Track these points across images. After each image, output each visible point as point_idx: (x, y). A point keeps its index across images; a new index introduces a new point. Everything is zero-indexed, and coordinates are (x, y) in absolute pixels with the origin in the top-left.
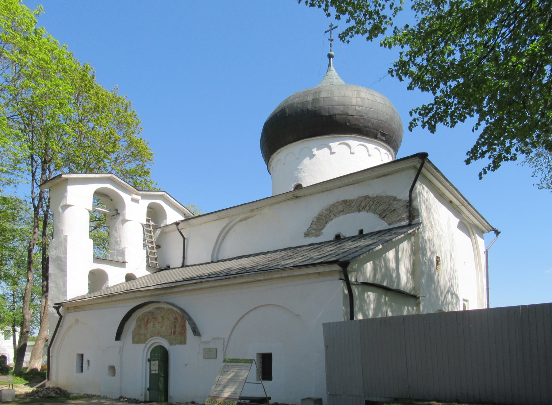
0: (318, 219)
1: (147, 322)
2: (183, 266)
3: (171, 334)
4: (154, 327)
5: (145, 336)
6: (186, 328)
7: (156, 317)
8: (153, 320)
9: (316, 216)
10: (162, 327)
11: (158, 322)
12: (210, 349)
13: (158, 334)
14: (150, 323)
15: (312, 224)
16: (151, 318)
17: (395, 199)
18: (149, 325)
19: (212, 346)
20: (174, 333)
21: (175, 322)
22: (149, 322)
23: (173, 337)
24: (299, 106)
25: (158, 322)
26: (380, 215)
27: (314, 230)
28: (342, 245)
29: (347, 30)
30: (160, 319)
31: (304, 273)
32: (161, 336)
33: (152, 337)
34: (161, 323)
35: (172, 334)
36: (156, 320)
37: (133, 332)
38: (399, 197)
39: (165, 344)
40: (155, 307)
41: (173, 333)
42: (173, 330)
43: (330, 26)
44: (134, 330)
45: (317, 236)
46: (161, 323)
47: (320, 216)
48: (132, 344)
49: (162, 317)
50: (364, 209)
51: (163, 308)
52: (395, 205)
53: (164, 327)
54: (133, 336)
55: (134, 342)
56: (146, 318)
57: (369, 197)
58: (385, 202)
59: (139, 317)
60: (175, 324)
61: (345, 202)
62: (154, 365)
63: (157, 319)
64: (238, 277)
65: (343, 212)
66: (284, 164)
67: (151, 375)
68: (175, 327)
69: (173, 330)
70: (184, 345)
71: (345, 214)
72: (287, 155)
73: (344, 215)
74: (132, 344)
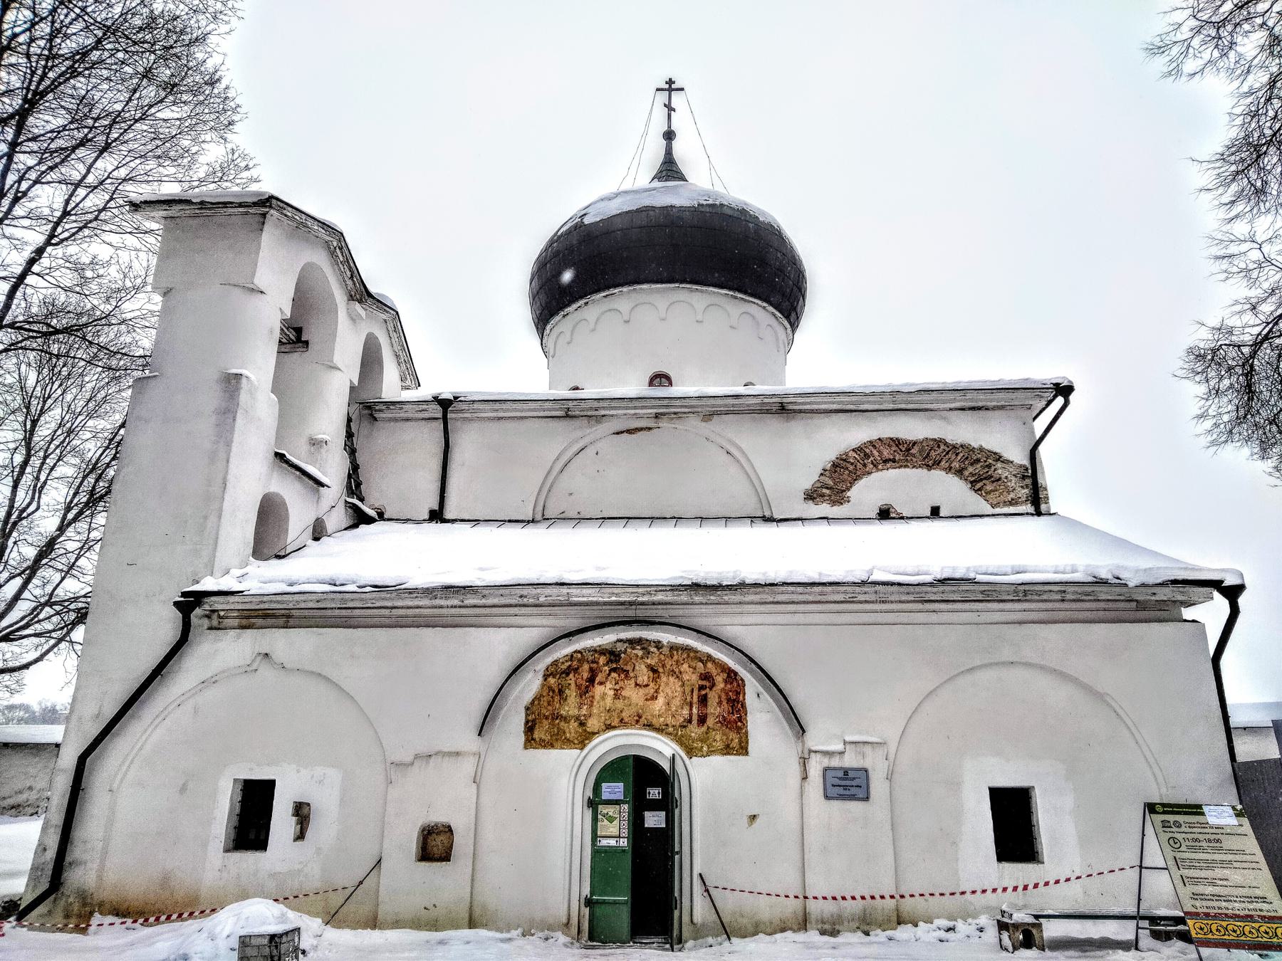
0: (835, 465)
1: (591, 680)
2: (437, 516)
3: (690, 721)
4: (617, 696)
5: (582, 724)
7: (629, 668)
8: (614, 675)
9: (834, 459)
10: (654, 698)
11: (637, 685)
12: (846, 772)
14: (601, 683)
15: (822, 474)
17: (998, 458)
18: (598, 690)
19: (850, 761)
20: (702, 720)
21: (701, 688)
22: (598, 680)
23: (695, 731)
25: (637, 685)
26: (973, 483)
27: (827, 488)
30: (643, 675)
32: (649, 726)
33: (609, 727)
35: (695, 721)
36: (627, 677)
38: (1007, 455)
39: (661, 748)
41: (695, 718)
42: (695, 711)
43: (667, 83)
45: (834, 503)
47: (842, 459)
48: (526, 748)
49: (653, 670)
50: (938, 465)
51: (658, 645)
52: (1001, 471)
53: (661, 700)
55: (531, 740)
56: (586, 667)
57: (946, 444)
58: (978, 461)
59: (555, 663)
60: (703, 692)
61: (897, 442)
62: (611, 819)
65: (889, 462)
66: (627, 322)
67: (597, 852)
68: (703, 701)
69: (695, 711)
70: (740, 759)
71: (899, 467)
72: (636, 306)
73: (897, 470)
74: (526, 748)
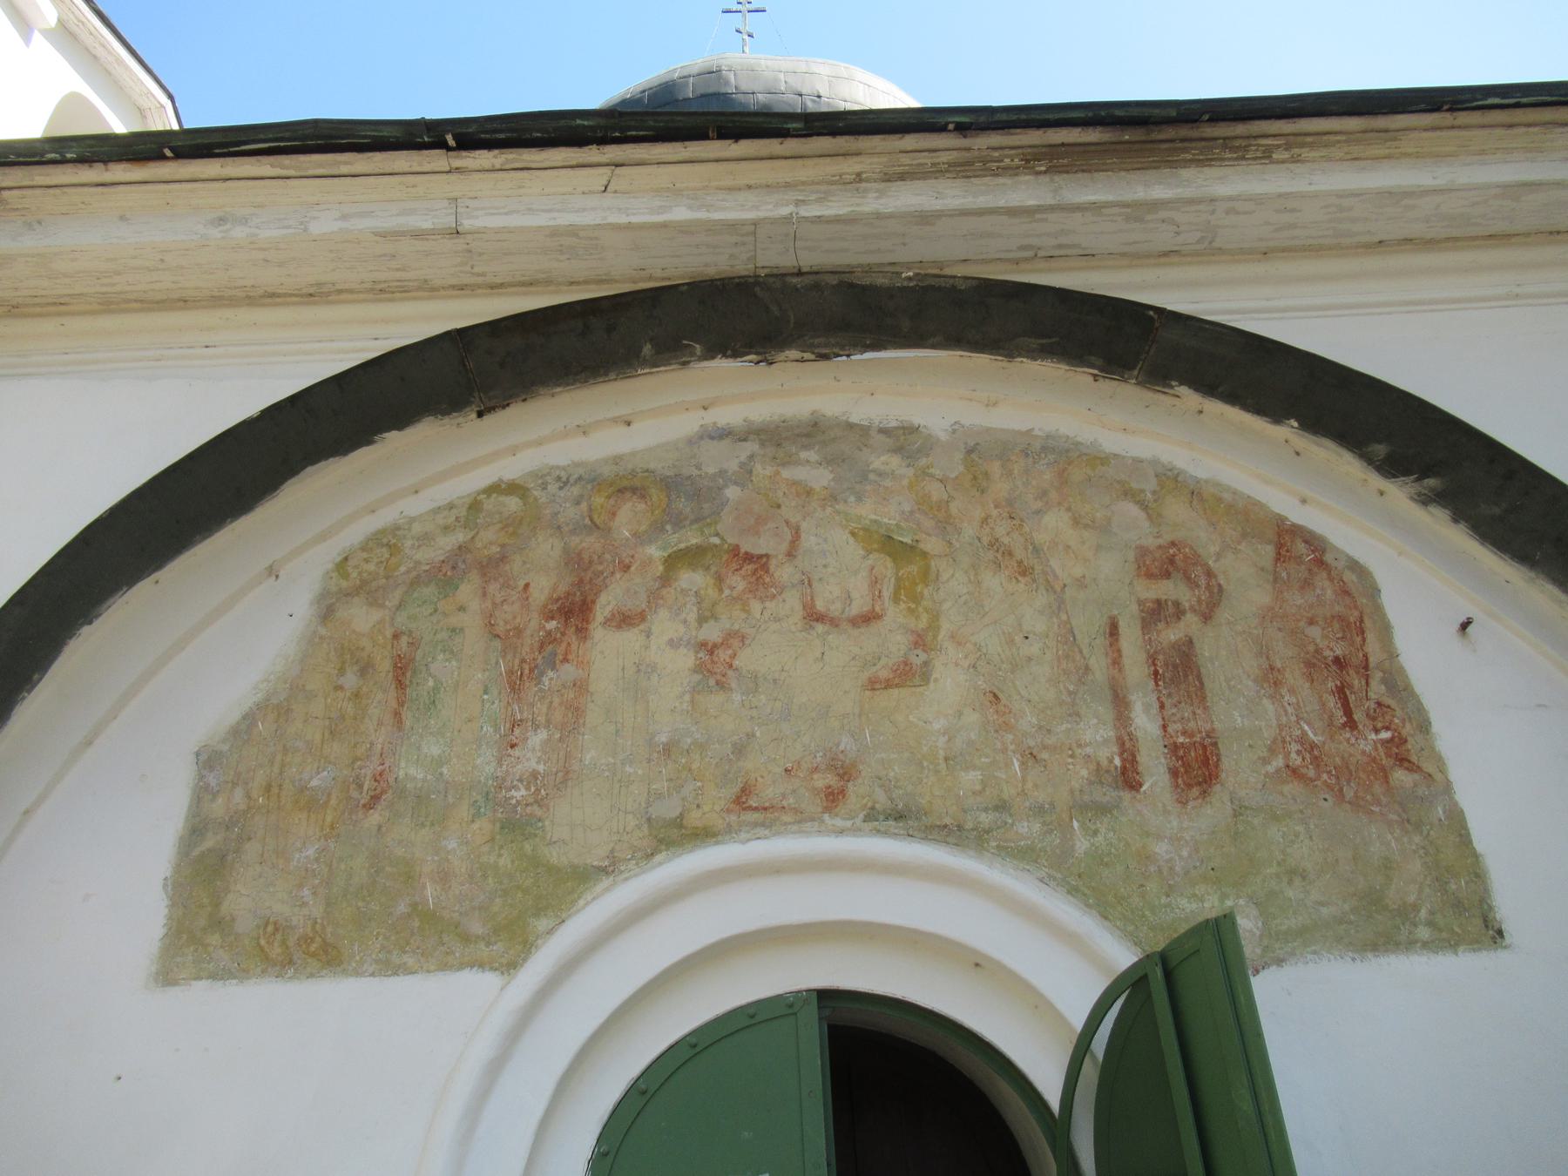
3: (1129, 777)
6: (1398, 684)
13: (833, 798)
14: (623, 620)
16: (655, 552)
24: (1077, 786)
25: (814, 617)
28: (399, 284)
29: (1119, 651)
31: (1002, 203)
34: (868, 618)
37: (208, 760)
40: (730, 415)
44: (243, 731)
46: (868, 618)
48: (166, 975)
51: (905, 439)
54: (196, 829)
56: (547, 548)
59: (387, 541)
60: (1171, 635)
63: (784, 573)
64: (25, 156)
74: (166, 975)
